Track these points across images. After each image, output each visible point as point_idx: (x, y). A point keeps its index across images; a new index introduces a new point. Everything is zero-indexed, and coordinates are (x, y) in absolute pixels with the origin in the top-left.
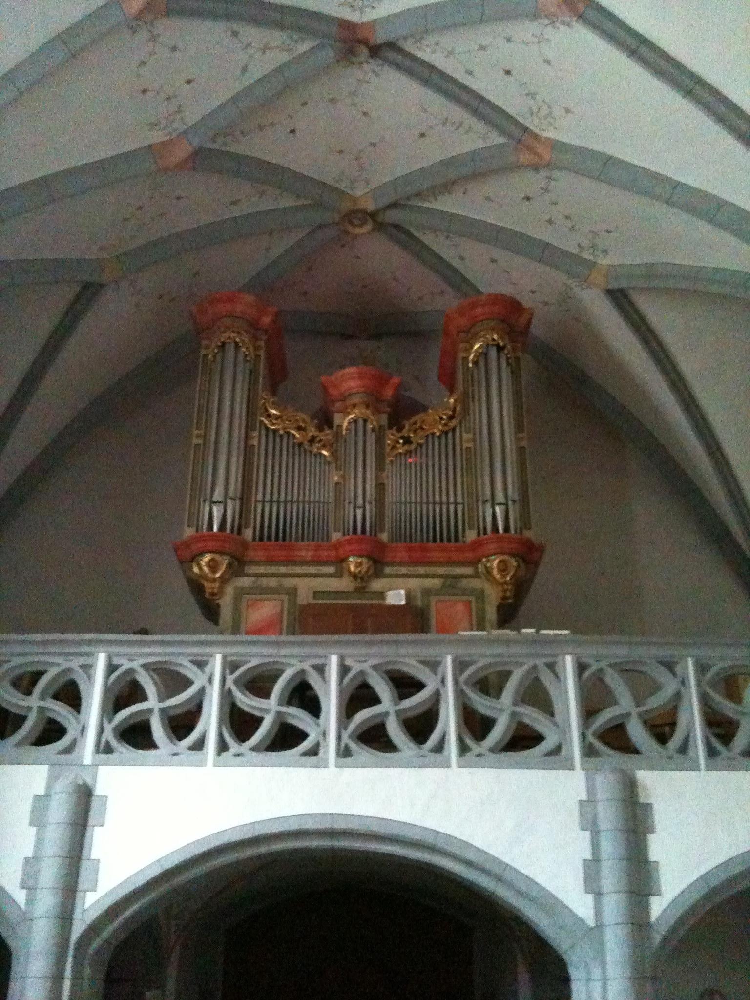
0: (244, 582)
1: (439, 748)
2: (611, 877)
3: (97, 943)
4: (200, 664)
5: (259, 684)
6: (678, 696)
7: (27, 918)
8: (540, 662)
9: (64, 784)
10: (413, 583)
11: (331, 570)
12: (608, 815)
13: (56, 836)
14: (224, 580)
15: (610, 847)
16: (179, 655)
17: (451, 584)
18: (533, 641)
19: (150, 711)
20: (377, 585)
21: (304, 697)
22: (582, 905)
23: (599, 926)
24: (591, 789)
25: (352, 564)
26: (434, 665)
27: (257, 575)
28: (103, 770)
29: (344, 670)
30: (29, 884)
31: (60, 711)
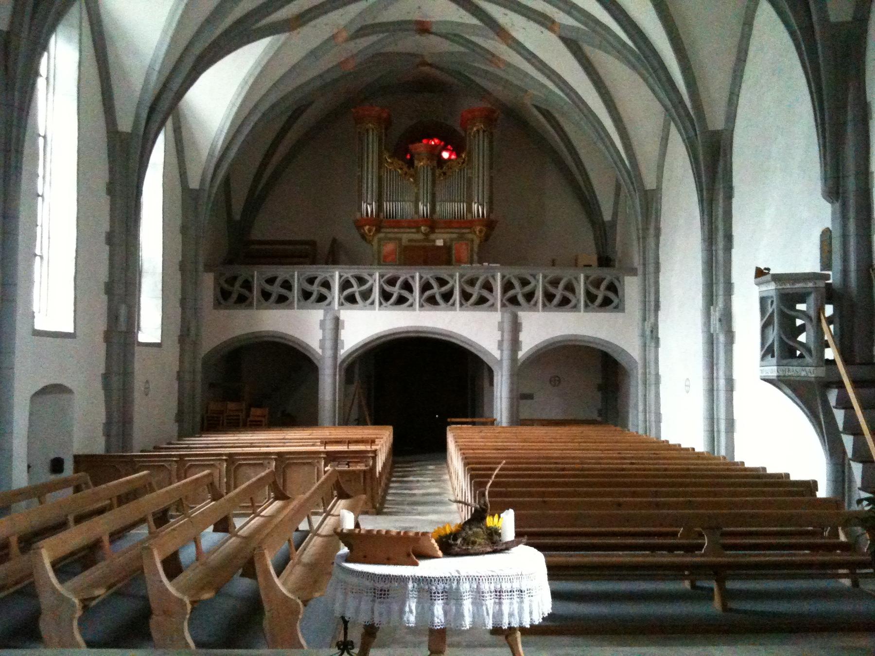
0: (381, 235)
1: (453, 304)
2: (506, 345)
3: (345, 364)
4: (371, 275)
5: (392, 282)
6: (536, 286)
7: (323, 358)
8: (489, 275)
9: (330, 317)
10: (446, 236)
11: (413, 230)
12: (507, 326)
13: (329, 335)
14: (374, 235)
15: (507, 336)
16: (364, 272)
17: (461, 237)
18: (488, 268)
19: (354, 292)
20: (432, 236)
21: (407, 286)
22: (497, 354)
23: (501, 360)
24: (502, 317)
25: (423, 228)
26: (452, 276)
27: (386, 233)
28: (342, 312)
29: (421, 278)
30: (322, 347)
31: (324, 291)
